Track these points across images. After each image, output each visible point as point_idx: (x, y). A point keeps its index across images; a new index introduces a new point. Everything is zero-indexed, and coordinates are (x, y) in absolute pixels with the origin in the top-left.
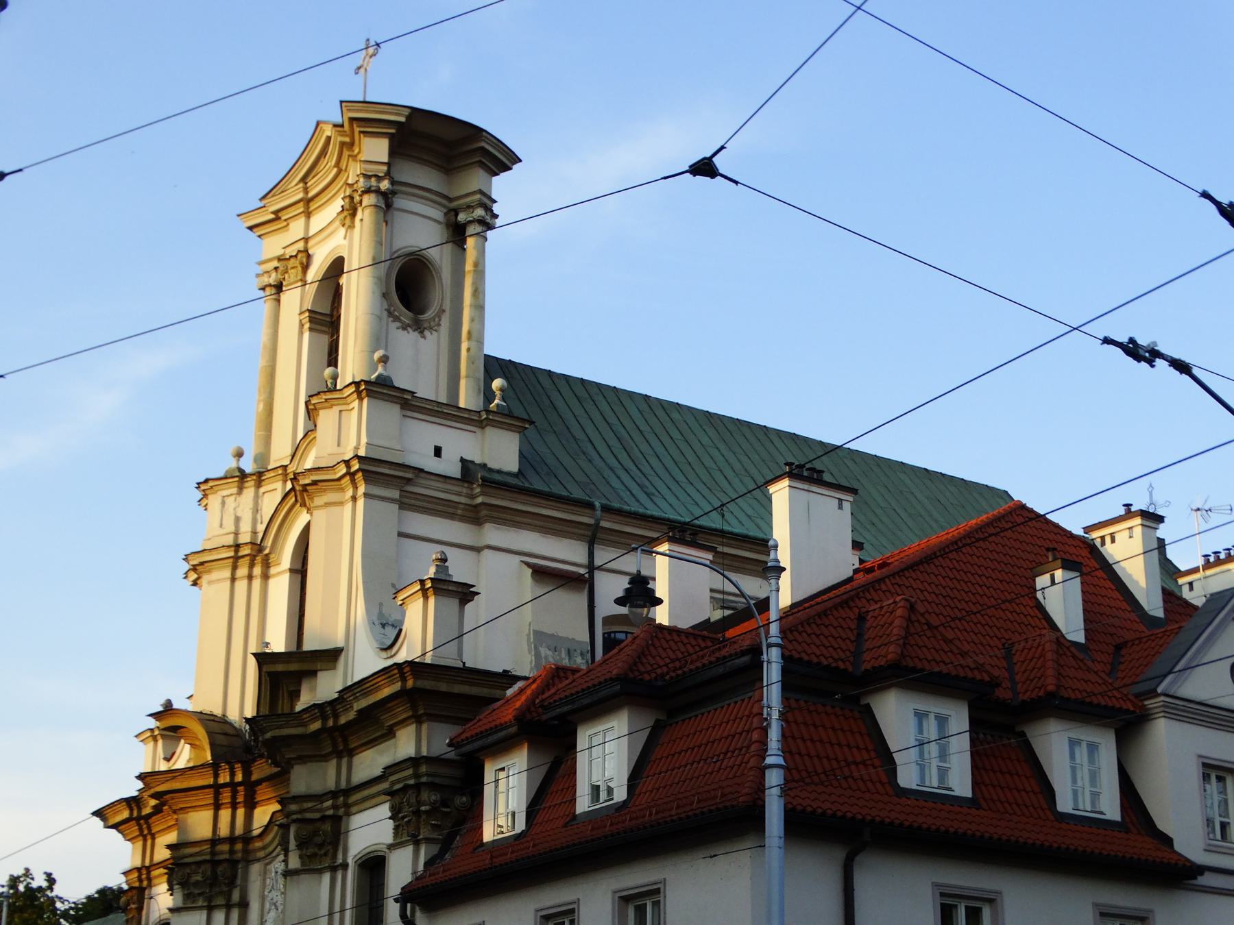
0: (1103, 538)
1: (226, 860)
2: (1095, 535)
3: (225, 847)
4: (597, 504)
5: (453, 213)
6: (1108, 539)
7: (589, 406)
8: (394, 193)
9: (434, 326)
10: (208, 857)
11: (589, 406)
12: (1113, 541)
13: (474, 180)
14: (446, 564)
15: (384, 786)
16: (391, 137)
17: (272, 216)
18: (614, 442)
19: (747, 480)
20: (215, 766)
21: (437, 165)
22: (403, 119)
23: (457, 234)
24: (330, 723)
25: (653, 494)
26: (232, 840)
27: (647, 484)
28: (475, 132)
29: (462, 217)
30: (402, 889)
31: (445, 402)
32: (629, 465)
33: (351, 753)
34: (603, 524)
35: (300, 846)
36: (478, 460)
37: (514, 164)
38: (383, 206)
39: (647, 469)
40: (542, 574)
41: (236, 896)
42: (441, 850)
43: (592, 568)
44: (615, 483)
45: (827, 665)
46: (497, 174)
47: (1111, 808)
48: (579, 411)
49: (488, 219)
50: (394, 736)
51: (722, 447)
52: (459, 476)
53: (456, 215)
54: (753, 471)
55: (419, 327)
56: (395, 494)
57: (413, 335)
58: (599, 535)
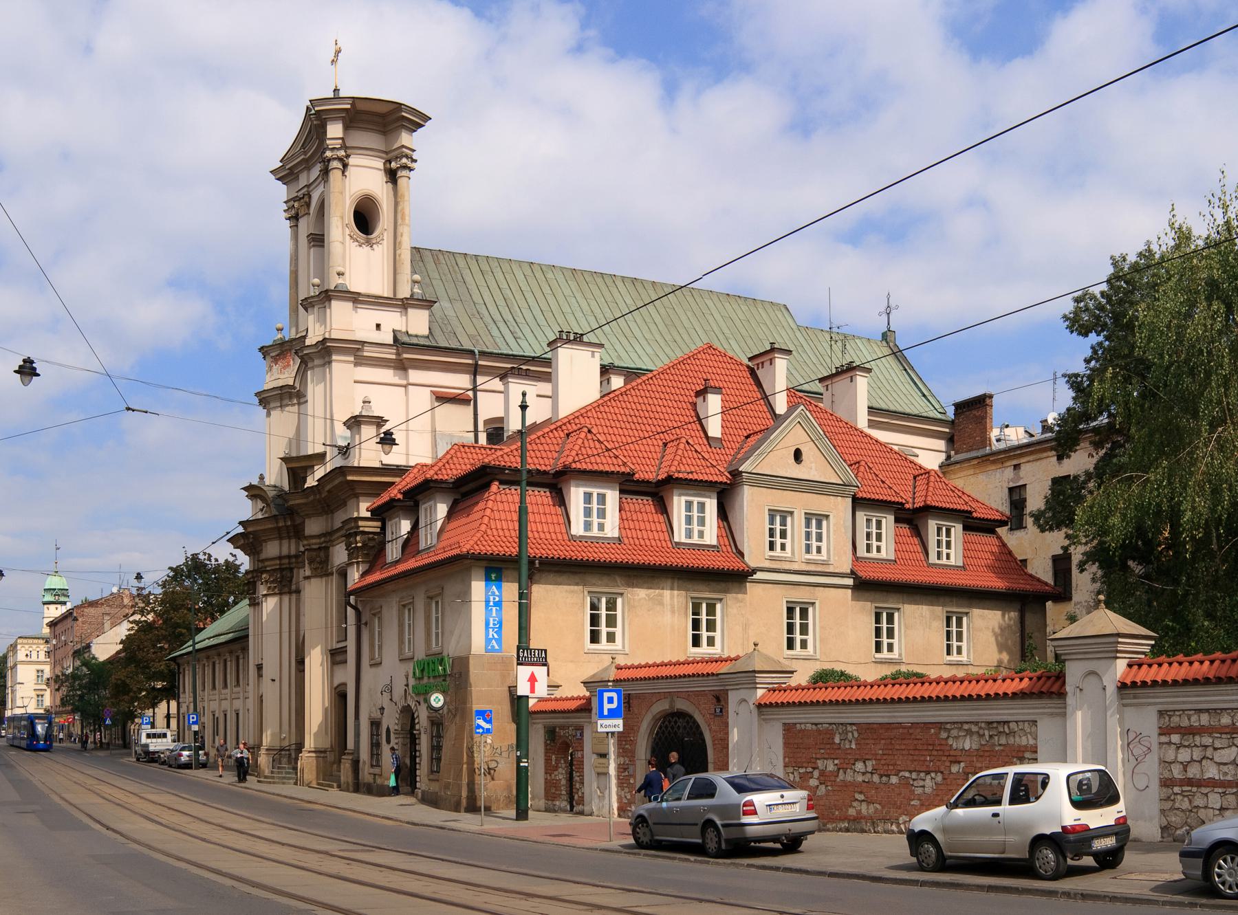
1: (286, 568)
3: (286, 561)
4: (476, 352)
6: (760, 366)
7: (490, 278)
8: (348, 156)
11: (490, 278)
12: (763, 367)
13: (405, 139)
15: (343, 532)
16: (343, 119)
18: (501, 303)
19: (592, 319)
21: (380, 131)
22: (349, 106)
23: (392, 176)
24: (318, 497)
25: (520, 338)
26: (289, 557)
27: (518, 330)
28: (399, 106)
29: (393, 165)
31: (386, 295)
32: (508, 317)
33: (332, 512)
34: (480, 363)
35: (310, 563)
37: (426, 122)
38: (341, 167)
39: (520, 320)
40: (443, 398)
41: (293, 587)
42: (370, 567)
43: (475, 389)
44: (495, 332)
46: (415, 131)
48: (481, 283)
49: (410, 164)
50: (346, 505)
51: (578, 295)
52: (392, 343)
53: (390, 163)
54: (597, 311)
55: (370, 244)
56: (352, 359)
57: (366, 249)
58: (478, 370)
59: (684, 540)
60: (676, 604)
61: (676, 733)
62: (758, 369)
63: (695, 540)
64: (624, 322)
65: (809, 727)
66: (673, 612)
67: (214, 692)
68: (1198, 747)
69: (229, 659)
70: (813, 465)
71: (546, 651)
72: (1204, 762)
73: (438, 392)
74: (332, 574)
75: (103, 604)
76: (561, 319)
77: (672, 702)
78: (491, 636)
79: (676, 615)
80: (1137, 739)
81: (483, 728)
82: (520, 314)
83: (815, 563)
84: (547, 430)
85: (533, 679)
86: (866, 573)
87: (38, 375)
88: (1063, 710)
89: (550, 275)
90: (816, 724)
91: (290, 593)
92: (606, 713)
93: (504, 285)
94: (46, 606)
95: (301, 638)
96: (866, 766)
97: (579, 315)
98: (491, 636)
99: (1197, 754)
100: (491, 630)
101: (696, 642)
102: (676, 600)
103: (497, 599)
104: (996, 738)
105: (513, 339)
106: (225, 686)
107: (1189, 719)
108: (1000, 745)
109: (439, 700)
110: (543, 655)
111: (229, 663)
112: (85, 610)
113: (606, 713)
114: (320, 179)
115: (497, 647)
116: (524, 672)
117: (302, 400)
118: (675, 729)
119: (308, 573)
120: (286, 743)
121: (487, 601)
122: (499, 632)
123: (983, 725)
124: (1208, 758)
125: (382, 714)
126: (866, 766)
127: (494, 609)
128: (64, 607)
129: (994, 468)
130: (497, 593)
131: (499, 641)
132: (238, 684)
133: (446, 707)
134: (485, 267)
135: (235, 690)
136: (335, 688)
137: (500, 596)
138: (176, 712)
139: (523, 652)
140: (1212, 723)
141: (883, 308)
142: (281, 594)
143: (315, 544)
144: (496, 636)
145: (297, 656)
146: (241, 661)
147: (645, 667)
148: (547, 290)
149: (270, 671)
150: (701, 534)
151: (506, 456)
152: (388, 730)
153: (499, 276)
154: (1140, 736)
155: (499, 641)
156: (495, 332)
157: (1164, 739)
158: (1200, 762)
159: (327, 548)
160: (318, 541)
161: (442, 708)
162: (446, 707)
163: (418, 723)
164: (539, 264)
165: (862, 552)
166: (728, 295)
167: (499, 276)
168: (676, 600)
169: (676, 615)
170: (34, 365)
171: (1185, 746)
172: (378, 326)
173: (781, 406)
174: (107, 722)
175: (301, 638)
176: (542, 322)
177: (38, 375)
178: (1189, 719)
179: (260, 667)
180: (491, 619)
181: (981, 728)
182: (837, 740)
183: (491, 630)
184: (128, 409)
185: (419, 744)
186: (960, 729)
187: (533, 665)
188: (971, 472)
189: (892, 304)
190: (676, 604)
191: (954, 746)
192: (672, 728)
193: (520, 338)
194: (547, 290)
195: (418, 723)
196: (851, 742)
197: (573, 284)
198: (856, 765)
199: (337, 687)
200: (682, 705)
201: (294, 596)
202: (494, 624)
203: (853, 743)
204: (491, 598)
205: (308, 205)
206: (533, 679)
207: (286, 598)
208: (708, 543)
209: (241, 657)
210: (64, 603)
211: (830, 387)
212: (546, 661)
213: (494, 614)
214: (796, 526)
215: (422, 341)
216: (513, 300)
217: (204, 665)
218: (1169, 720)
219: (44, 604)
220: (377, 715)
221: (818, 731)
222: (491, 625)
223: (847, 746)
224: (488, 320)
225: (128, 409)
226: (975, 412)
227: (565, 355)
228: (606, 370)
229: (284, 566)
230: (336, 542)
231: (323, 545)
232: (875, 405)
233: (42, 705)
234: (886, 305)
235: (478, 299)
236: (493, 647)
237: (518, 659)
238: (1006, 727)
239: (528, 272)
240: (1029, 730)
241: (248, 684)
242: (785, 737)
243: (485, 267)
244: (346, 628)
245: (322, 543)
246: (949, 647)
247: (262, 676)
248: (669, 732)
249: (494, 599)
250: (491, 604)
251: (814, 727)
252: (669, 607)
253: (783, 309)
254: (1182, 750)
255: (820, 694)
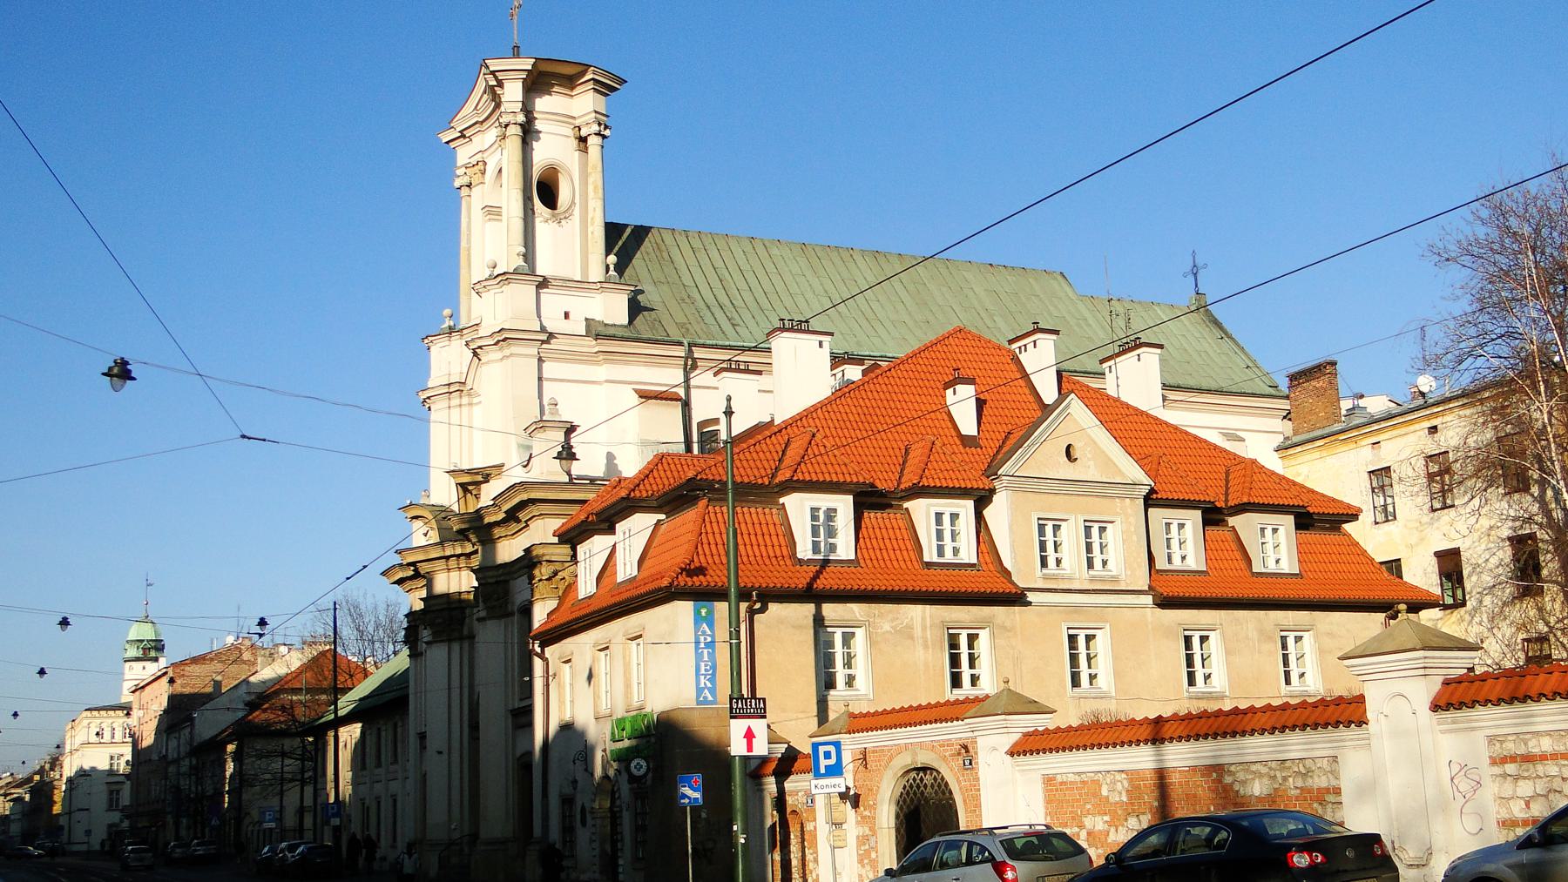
0: (1020, 348)
2: (1015, 346)
5: (577, 129)
6: (1023, 348)
9: (567, 216)
10: (445, 606)
12: (1025, 350)
14: (557, 407)
17: (459, 134)
20: (441, 543)
25: (738, 325)
27: (737, 317)
30: (992, 501)
35: (483, 601)
36: (598, 318)
40: (646, 396)
41: (466, 632)
44: (709, 319)
45: (749, 483)
47: (968, 554)
48: (692, 262)
51: (809, 273)
59: (935, 559)
60: (929, 636)
61: (922, 793)
62: (1020, 353)
63: (949, 557)
64: (446, 578)
65: (1072, 778)
66: (926, 647)
67: (364, 773)
68: (1541, 778)
69: (384, 728)
70: (1092, 463)
71: (764, 700)
72: (1551, 796)
73: (641, 390)
74: (512, 614)
75: (212, 659)
76: (788, 302)
77: (915, 754)
78: (702, 685)
79: (930, 650)
80: (1462, 773)
81: (689, 798)
82: (739, 297)
83: (1102, 580)
84: (752, 442)
85: (749, 735)
86: (1167, 591)
87: (134, 379)
88: (1367, 742)
89: (775, 251)
90: (1079, 774)
91: (461, 639)
92: (823, 771)
93: (719, 264)
94: (128, 664)
95: (476, 697)
96: (1140, 821)
97: (809, 295)
98: (702, 685)
99: (1540, 787)
100: (702, 677)
101: (956, 681)
102: (929, 633)
103: (709, 639)
104: (1291, 779)
105: (731, 327)
106: (379, 765)
107: (1526, 744)
108: (1296, 788)
109: (641, 767)
110: (762, 705)
111: (383, 734)
112: (187, 668)
113: (823, 771)
114: (496, 145)
115: (710, 698)
116: (738, 727)
117: (475, 400)
118: (922, 788)
119: (483, 614)
120: (456, 835)
121: (697, 643)
122: (713, 679)
123: (1273, 765)
124: (1556, 791)
125: (575, 789)
126: (1140, 821)
127: (706, 651)
128: (155, 664)
129: (1346, 448)
130: (709, 632)
131: (713, 691)
132: (395, 761)
133: (650, 775)
134: (697, 244)
135: (392, 768)
136: (518, 759)
137: (713, 636)
138: (311, 804)
139: (737, 703)
140: (1556, 748)
141: (1188, 266)
142: (450, 641)
143: (492, 577)
144: (709, 685)
145: (470, 720)
146: (399, 730)
147: (926, 707)
148: (770, 268)
149: (436, 741)
150: (956, 551)
151: (716, 470)
152: (583, 809)
153: (714, 254)
154: (1466, 768)
155: (713, 691)
156: (709, 319)
157: (1497, 770)
158: (1546, 796)
159: (507, 582)
160: (496, 573)
161: (645, 775)
162: (650, 775)
163: (619, 797)
164: (762, 240)
165: (1161, 564)
166: (991, 265)
167: (714, 254)
168: (929, 633)
169: (930, 650)
170: (129, 367)
171: (1525, 778)
172: (567, 315)
173: (1049, 393)
174: (213, 822)
175: (476, 697)
176: (765, 304)
177: (134, 379)
178: (1526, 744)
179: (422, 736)
180: (702, 664)
181: (1270, 769)
182: (1105, 792)
183: (702, 677)
184: (243, 436)
185: (621, 824)
186: (1247, 771)
187: (749, 717)
188: (1317, 454)
189: (1199, 262)
190: (929, 636)
191: (1242, 792)
192: (918, 787)
193: (738, 325)
194: (770, 268)
195: (619, 797)
196: (1121, 793)
197: (803, 262)
198: (1129, 822)
199: (521, 757)
200: (924, 759)
201: (466, 645)
202: (706, 670)
203: (1124, 794)
204: (702, 638)
205: (483, 173)
206: (749, 735)
207: (456, 647)
208: (966, 561)
209: (400, 724)
210: (156, 660)
211: (1113, 368)
212: (765, 712)
213: (706, 658)
214: (1071, 536)
215: (620, 333)
216: (730, 280)
217: (379, 729)
218: (1501, 748)
219: (125, 661)
220: (568, 790)
221: (1083, 782)
222: (703, 672)
223: (1117, 799)
224: (701, 304)
225: (243, 436)
226: (1314, 383)
227: (784, 345)
228: (837, 360)
229: (454, 606)
230: (518, 574)
231: (502, 578)
232: (1172, 382)
233: (117, 805)
234: (1192, 264)
235: (687, 280)
236: (705, 698)
237: (731, 712)
238: (1301, 765)
239: (749, 248)
240: (1328, 769)
241: (408, 760)
242: (1047, 791)
243: (697, 244)
244: (731, 639)
245: (500, 576)
246: (1287, 674)
247: (425, 748)
248: (915, 793)
249: (705, 639)
250: (702, 645)
251: (1077, 778)
252: (921, 641)
253: (1060, 278)
254: (1521, 783)
255: (1125, 733)
